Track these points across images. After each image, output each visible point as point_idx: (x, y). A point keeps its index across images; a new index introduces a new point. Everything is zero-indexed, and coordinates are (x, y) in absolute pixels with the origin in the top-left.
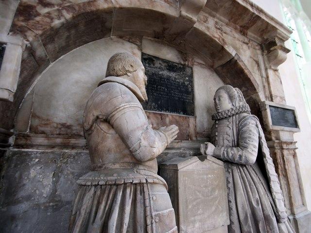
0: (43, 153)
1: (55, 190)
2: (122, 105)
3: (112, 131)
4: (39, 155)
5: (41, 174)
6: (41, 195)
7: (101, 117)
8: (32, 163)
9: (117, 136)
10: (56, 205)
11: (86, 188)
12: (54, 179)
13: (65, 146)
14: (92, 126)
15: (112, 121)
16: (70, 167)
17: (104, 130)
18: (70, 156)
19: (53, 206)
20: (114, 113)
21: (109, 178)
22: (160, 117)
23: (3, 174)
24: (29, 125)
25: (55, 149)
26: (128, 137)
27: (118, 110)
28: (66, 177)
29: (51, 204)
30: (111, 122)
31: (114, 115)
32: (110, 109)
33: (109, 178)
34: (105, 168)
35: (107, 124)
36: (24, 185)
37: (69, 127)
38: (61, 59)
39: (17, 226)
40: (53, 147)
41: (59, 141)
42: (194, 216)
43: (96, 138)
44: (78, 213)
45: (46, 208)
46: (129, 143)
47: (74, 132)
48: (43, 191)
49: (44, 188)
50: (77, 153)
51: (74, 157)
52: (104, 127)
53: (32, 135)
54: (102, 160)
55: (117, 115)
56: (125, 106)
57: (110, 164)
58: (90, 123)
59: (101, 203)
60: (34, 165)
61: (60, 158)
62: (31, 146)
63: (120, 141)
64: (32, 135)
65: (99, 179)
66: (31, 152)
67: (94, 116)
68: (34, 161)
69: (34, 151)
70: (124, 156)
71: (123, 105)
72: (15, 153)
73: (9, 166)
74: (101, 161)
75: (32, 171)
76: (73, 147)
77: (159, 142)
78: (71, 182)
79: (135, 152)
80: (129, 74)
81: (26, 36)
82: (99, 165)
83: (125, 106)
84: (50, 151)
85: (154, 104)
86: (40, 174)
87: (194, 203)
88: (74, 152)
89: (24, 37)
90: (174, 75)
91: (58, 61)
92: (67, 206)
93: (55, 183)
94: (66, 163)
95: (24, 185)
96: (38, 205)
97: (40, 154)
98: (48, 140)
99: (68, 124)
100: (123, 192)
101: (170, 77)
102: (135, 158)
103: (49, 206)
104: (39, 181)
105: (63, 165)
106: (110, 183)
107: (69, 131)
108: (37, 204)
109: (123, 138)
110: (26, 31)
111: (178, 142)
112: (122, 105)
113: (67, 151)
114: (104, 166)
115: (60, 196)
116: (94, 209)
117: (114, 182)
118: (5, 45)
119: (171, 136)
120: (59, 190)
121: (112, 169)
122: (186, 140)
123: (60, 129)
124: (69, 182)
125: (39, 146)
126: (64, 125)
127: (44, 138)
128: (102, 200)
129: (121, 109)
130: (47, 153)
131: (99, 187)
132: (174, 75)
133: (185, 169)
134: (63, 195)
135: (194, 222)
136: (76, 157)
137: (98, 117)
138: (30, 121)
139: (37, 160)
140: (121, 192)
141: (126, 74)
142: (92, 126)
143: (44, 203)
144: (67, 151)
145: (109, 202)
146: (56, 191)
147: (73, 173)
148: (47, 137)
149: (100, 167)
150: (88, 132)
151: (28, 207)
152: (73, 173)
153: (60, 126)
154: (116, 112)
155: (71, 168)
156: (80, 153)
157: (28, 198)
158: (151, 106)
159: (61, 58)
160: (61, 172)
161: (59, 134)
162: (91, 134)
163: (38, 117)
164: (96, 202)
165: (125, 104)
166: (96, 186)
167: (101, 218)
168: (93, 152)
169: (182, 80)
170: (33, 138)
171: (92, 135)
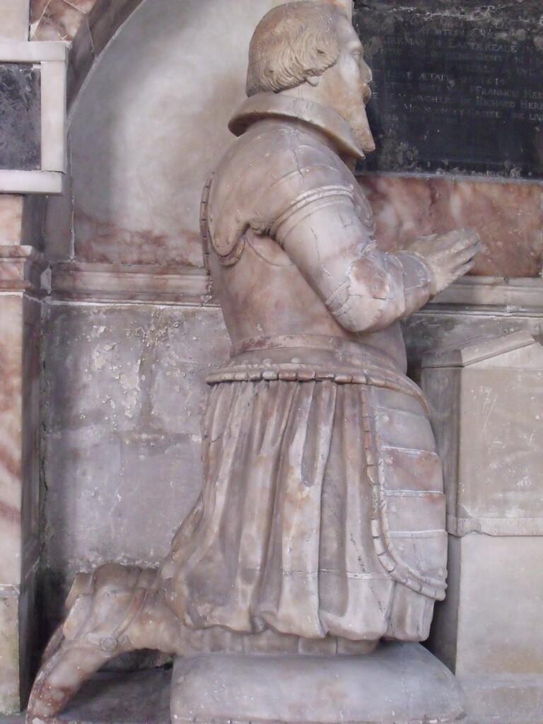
0: (111, 311)
1: (147, 406)
2: (301, 197)
3: (283, 259)
4: (104, 317)
5: (115, 364)
6: (121, 410)
7: (255, 225)
8: (93, 335)
9: (294, 269)
10: (155, 440)
11: (235, 388)
12: (143, 378)
13: (158, 294)
14: (235, 248)
15: (282, 234)
16: (176, 351)
17: (263, 255)
18: (169, 321)
19: (148, 441)
20: (284, 217)
21: (284, 366)
22: (424, 192)
23: (43, 359)
24: (73, 242)
25: (137, 303)
26: (320, 273)
27: (294, 208)
28: (168, 373)
29: (144, 436)
30: (278, 235)
31: (286, 220)
32: (275, 207)
33: (284, 366)
34: (272, 346)
35: (271, 241)
36: (85, 386)
37: (158, 241)
38: (115, 41)
39: (84, 474)
40: (132, 297)
41: (141, 279)
42: (504, 491)
43: (244, 275)
44: (226, 433)
45: (136, 443)
46: (322, 287)
47: (173, 254)
48: (123, 403)
49: (125, 395)
50: (186, 314)
51: (181, 325)
52: (263, 247)
53: (83, 265)
54: (262, 327)
55: (292, 221)
56: (308, 196)
57: (281, 338)
58: (231, 239)
59: (271, 414)
60: (96, 341)
61: (149, 325)
62: (86, 295)
63: (301, 282)
64: (83, 265)
65: (262, 366)
66: (86, 308)
67: (238, 222)
68: (97, 330)
69: (93, 307)
70: (315, 320)
71: (305, 195)
72: (56, 312)
73: (51, 341)
74: (260, 329)
75: (95, 354)
76: (177, 298)
77: (395, 286)
78: (181, 389)
79: (337, 308)
80: (313, 79)
81: (62, 26)
82: (257, 338)
83: (308, 196)
84: (125, 305)
85: (404, 145)
86: (113, 364)
87: (508, 459)
88: (178, 310)
89: (60, 31)
90: (486, 14)
91: (111, 47)
92: (178, 445)
93: (147, 386)
94: (165, 338)
95: (85, 386)
96: (117, 436)
97: (105, 313)
98: (118, 277)
99: (157, 232)
100: (315, 398)
101: (468, 26)
102: (339, 325)
103: (140, 441)
104: (113, 380)
105: (159, 344)
106: (287, 375)
107: (160, 252)
108: (115, 433)
109: (310, 277)
110: (62, 14)
111: (493, 285)
112: (301, 197)
113: (162, 307)
114: (269, 342)
115: (160, 420)
116: (258, 427)
117: (294, 375)
118: (35, 67)
119: (451, 266)
120: (155, 406)
121: (286, 349)
122: (528, 275)
123: (140, 246)
124: (177, 388)
125: (101, 294)
126: (147, 237)
127: (108, 275)
128: (273, 408)
129: (299, 205)
130: (120, 311)
131: (263, 382)
132: (486, 14)
133: (484, 364)
134: (167, 419)
135: (503, 505)
136: (186, 325)
137: (247, 226)
138: (73, 231)
139: (102, 329)
140: (311, 398)
141: (305, 80)
142: (235, 248)
143: (129, 432)
144: (162, 307)
145: (289, 423)
146: (151, 408)
147: (182, 366)
148: (116, 271)
149: (260, 343)
150: (222, 265)
151: (100, 436)
152: (182, 366)
153: (137, 240)
154: (289, 213)
155: (178, 356)
156: (193, 314)
157: (98, 416)
158: (393, 153)
159: (117, 33)
160: (156, 360)
161: (140, 262)
162: (232, 266)
163: (89, 219)
164: (259, 414)
165: (310, 192)
166: (255, 381)
167: (273, 442)
168: (237, 310)
169: (520, 33)
170: (86, 273)
171: (237, 267)
